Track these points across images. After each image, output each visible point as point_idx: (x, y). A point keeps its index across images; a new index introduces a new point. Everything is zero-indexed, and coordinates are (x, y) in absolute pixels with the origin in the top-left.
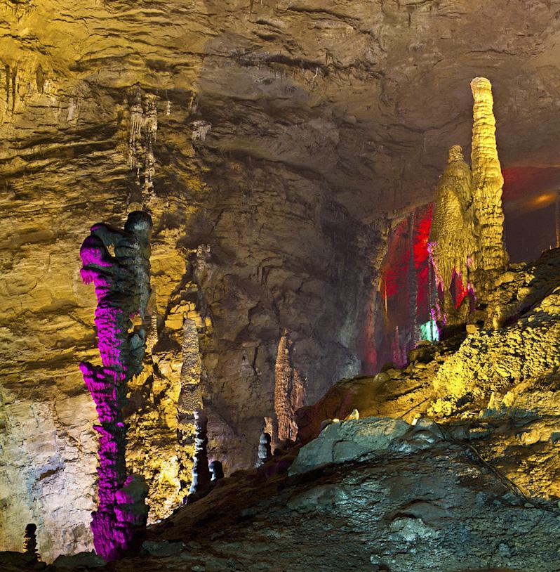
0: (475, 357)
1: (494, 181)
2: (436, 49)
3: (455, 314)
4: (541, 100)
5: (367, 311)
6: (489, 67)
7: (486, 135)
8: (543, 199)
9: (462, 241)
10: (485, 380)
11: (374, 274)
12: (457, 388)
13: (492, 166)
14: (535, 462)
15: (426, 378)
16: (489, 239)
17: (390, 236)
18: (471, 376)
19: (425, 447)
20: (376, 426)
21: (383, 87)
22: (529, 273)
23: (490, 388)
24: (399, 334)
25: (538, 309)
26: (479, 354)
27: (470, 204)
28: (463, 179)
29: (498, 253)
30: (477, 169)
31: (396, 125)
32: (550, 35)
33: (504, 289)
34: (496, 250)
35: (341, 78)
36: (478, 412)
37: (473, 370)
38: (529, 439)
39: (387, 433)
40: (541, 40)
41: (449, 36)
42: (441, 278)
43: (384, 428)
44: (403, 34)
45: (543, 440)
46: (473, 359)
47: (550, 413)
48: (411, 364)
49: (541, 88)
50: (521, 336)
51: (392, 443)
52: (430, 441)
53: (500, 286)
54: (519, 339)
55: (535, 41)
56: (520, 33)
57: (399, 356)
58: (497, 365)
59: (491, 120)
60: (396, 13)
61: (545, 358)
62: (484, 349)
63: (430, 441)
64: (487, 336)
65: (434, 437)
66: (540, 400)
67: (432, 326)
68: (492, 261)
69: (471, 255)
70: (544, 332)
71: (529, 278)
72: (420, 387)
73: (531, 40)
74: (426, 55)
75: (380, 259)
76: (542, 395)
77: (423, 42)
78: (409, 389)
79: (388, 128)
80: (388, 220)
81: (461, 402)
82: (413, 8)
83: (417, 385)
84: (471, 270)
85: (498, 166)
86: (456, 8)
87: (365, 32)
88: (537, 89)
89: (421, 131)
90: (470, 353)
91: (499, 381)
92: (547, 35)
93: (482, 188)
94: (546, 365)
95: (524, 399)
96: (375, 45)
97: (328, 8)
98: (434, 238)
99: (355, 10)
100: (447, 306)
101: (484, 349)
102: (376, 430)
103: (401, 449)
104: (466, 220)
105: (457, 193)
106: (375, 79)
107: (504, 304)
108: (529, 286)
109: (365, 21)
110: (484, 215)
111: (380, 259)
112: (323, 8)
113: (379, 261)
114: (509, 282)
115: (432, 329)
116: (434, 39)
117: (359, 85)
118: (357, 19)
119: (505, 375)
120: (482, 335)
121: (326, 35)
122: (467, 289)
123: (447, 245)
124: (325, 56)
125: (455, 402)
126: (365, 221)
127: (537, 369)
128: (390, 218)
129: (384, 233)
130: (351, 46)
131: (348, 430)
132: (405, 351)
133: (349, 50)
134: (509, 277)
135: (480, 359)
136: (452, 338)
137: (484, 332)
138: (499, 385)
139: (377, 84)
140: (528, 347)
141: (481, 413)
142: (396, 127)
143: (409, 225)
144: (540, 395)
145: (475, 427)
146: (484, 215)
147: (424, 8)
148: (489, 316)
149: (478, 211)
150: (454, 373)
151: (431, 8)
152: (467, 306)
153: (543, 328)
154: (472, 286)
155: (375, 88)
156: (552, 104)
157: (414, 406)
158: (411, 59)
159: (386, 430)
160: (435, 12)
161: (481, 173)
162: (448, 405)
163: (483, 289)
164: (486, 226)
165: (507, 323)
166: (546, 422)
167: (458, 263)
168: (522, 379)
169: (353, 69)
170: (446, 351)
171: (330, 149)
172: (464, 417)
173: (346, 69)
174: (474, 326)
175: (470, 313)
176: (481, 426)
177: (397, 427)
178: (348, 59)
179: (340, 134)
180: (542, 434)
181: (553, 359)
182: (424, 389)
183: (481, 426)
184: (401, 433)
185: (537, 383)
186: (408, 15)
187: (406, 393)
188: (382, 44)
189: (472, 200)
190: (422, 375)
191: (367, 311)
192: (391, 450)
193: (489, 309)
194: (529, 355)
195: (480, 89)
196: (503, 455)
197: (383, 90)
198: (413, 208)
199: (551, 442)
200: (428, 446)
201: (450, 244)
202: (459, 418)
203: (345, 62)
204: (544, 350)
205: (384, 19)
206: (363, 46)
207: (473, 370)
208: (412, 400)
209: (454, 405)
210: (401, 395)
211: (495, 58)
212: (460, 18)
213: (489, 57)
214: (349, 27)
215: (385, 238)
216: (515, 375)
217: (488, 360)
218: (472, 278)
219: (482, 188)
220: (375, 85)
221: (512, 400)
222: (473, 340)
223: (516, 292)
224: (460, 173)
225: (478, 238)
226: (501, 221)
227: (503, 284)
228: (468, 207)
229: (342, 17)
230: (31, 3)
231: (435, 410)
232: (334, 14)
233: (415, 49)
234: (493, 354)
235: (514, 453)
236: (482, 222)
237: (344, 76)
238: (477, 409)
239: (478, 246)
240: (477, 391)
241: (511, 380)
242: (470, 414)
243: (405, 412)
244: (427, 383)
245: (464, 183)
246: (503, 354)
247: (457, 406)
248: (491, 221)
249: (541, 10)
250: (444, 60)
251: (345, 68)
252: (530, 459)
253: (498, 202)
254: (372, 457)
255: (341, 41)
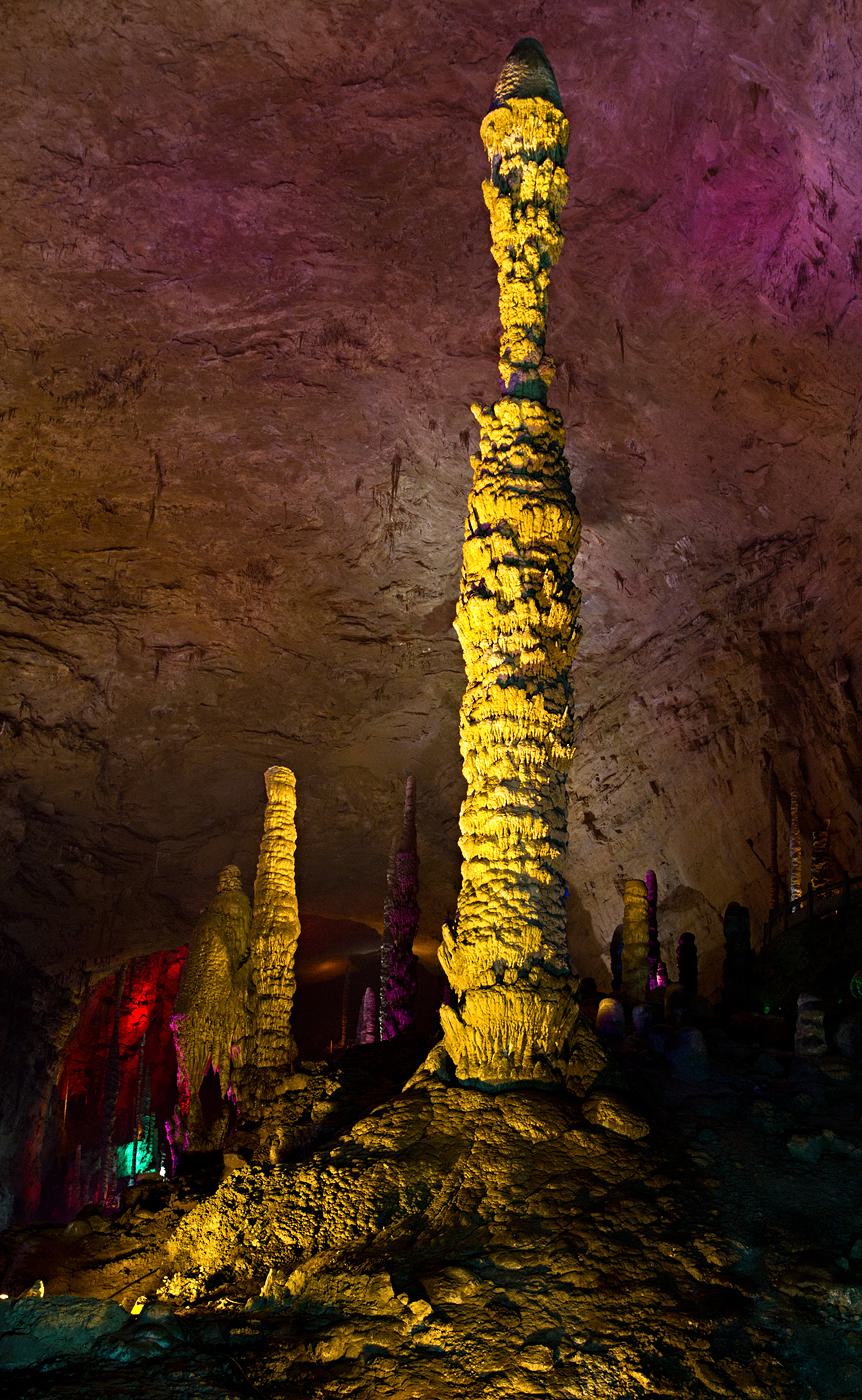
0: (241, 1207)
1: (286, 928)
2: (192, 720)
3: (204, 1132)
4: (342, 816)
5: (34, 1116)
6: (268, 756)
7: (280, 855)
8: (327, 966)
9: (225, 1017)
10: (255, 1248)
11: (52, 1056)
12: (208, 1256)
13: (285, 904)
14: (336, 1392)
15: (153, 1235)
16: (269, 1019)
17: (85, 999)
18: (233, 1239)
19: (154, 1353)
20: (73, 1313)
21: (104, 766)
22: (333, 1080)
23: (262, 1262)
24: (83, 1158)
25: (346, 1139)
26: (248, 1204)
27: (245, 960)
28: (238, 919)
29: (282, 1042)
30: (262, 906)
31: (116, 826)
32: (363, 722)
33: (291, 1101)
34: (279, 1037)
35: (39, 743)
36: (244, 1301)
37: (237, 1229)
38: (329, 1354)
39: (91, 1325)
40: (350, 728)
41: (213, 702)
42: (188, 1076)
43: (86, 1315)
44: (145, 688)
45: (349, 1355)
46: (238, 1212)
47: (362, 1311)
48: (129, 1211)
49: (344, 798)
50: (318, 1179)
51: (98, 1343)
52: (163, 1344)
53: (284, 1095)
54: (314, 1184)
55: (341, 728)
56: (321, 713)
57: (78, 1196)
58: (276, 1225)
59: (291, 834)
60: (137, 657)
61: (354, 1219)
62: (256, 1196)
63: (163, 1344)
64: (262, 1174)
65: (169, 1338)
66: (348, 1288)
67: (135, 1150)
68: (271, 1055)
69: (239, 1041)
70: (356, 1176)
71: (331, 1087)
72: (142, 1250)
73: (335, 725)
74: (175, 726)
75: (65, 1033)
76: (351, 1280)
77: (174, 706)
78: (123, 1252)
79: (104, 829)
80: (84, 973)
81: (213, 1281)
82: (164, 653)
83: (138, 1246)
84: (236, 1066)
85: (295, 906)
86: (230, 662)
87: (86, 678)
88: (337, 800)
89: (154, 840)
90: (233, 1201)
91: (279, 1251)
92: (359, 722)
93: (266, 937)
94: (355, 1230)
95: (321, 1285)
96: (100, 701)
97: (34, 634)
98: (184, 1007)
99: (75, 643)
100: (192, 1121)
101: (256, 1196)
102: (72, 1319)
103: (113, 1356)
104: (235, 984)
105: (227, 939)
106: (93, 752)
107: (288, 1124)
108: (331, 1100)
109: (88, 661)
110: (265, 980)
111: (65, 1033)
112: (27, 632)
113: (61, 1038)
114: (299, 1091)
115: (135, 1155)
116: (191, 703)
117: (67, 758)
118: (77, 657)
119: (288, 1240)
120: (254, 1172)
121: (26, 673)
122: (226, 1096)
123: (202, 1021)
124: (19, 706)
125: (204, 1280)
126: (48, 971)
127: (340, 1236)
128: (87, 970)
129: (76, 992)
130: (63, 696)
131: (25, 1315)
132: (87, 1187)
133: (58, 701)
134: (299, 1083)
135: (249, 1212)
136: (197, 1177)
137: (259, 1168)
138: (277, 1258)
139: (94, 760)
140: (329, 1198)
141: (249, 1303)
142: (116, 830)
143: (117, 986)
144: (348, 1279)
145: (239, 1327)
146: (265, 980)
147: (181, 655)
148: (262, 1141)
149: (256, 973)
150: (204, 1232)
151: (191, 656)
152: (224, 1122)
153: (355, 1170)
154: (235, 1091)
155: (90, 764)
156: (357, 824)
157: (130, 1281)
158: (152, 729)
159: (89, 1320)
160: (196, 663)
161: (267, 913)
162: (193, 1285)
163: (252, 1097)
164: (267, 997)
165: (293, 1158)
166: (356, 1325)
167: (217, 1052)
168: (315, 1251)
169: (61, 731)
170: (188, 1193)
171: (7, 850)
172: (219, 1307)
173: (50, 731)
174: (236, 1156)
175: (227, 1134)
176: (250, 1325)
177: (109, 1316)
178: (55, 715)
179: (27, 829)
180: (349, 1346)
181: (367, 1222)
182: (150, 1254)
183: (250, 1325)
184: (115, 1326)
185: (340, 1259)
186: (155, 662)
187: (118, 1259)
188: (110, 700)
189: (249, 954)
190: (145, 1230)
191: (34, 1116)
192: (96, 1356)
193: (264, 1132)
194: (329, 1212)
195: (279, 783)
196: (285, 1377)
197: (103, 769)
198: (126, 958)
199: (362, 1361)
200: (157, 1353)
201: (207, 1020)
202: (211, 1308)
203: (50, 719)
204: (353, 1206)
205: (118, 662)
206: (80, 698)
207: (237, 1229)
208: (127, 1271)
209: (201, 1285)
210: (109, 1261)
211: (279, 744)
212: (234, 678)
213: (270, 742)
214: (62, 667)
215: (77, 1002)
216: (304, 1242)
217: (262, 1214)
218: (237, 1078)
219: (266, 937)
220: (91, 761)
221: (301, 1283)
222: (240, 1180)
223: (310, 1107)
224: (234, 910)
225: (252, 1015)
226: (290, 992)
227: (288, 1092)
228: (241, 965)
229: (54, 651)
230: (3, 509)
231: (171, 1292)
232: (42, 644)
233: (160, 714)
234: (271, 1205)
235: (304, 1376)
236: (262, 989)
237: (44, 740)
238: (240, 1296)
239: (251, 1029)
240: (240, 1265)
241: (297, 1250)
242: (229, 1304)
243: (115, 1291)
244: (154, 1245)
245: (239, 926)
246: (287, 1206)
247: (207, 1289)
248: (275, 990)
249: (355, 683)
250: (202, 737)
251: (48, 728)
252: (329, 1388)
253: (289, 960)
254: (63, 1365)
255: (47, 686)
